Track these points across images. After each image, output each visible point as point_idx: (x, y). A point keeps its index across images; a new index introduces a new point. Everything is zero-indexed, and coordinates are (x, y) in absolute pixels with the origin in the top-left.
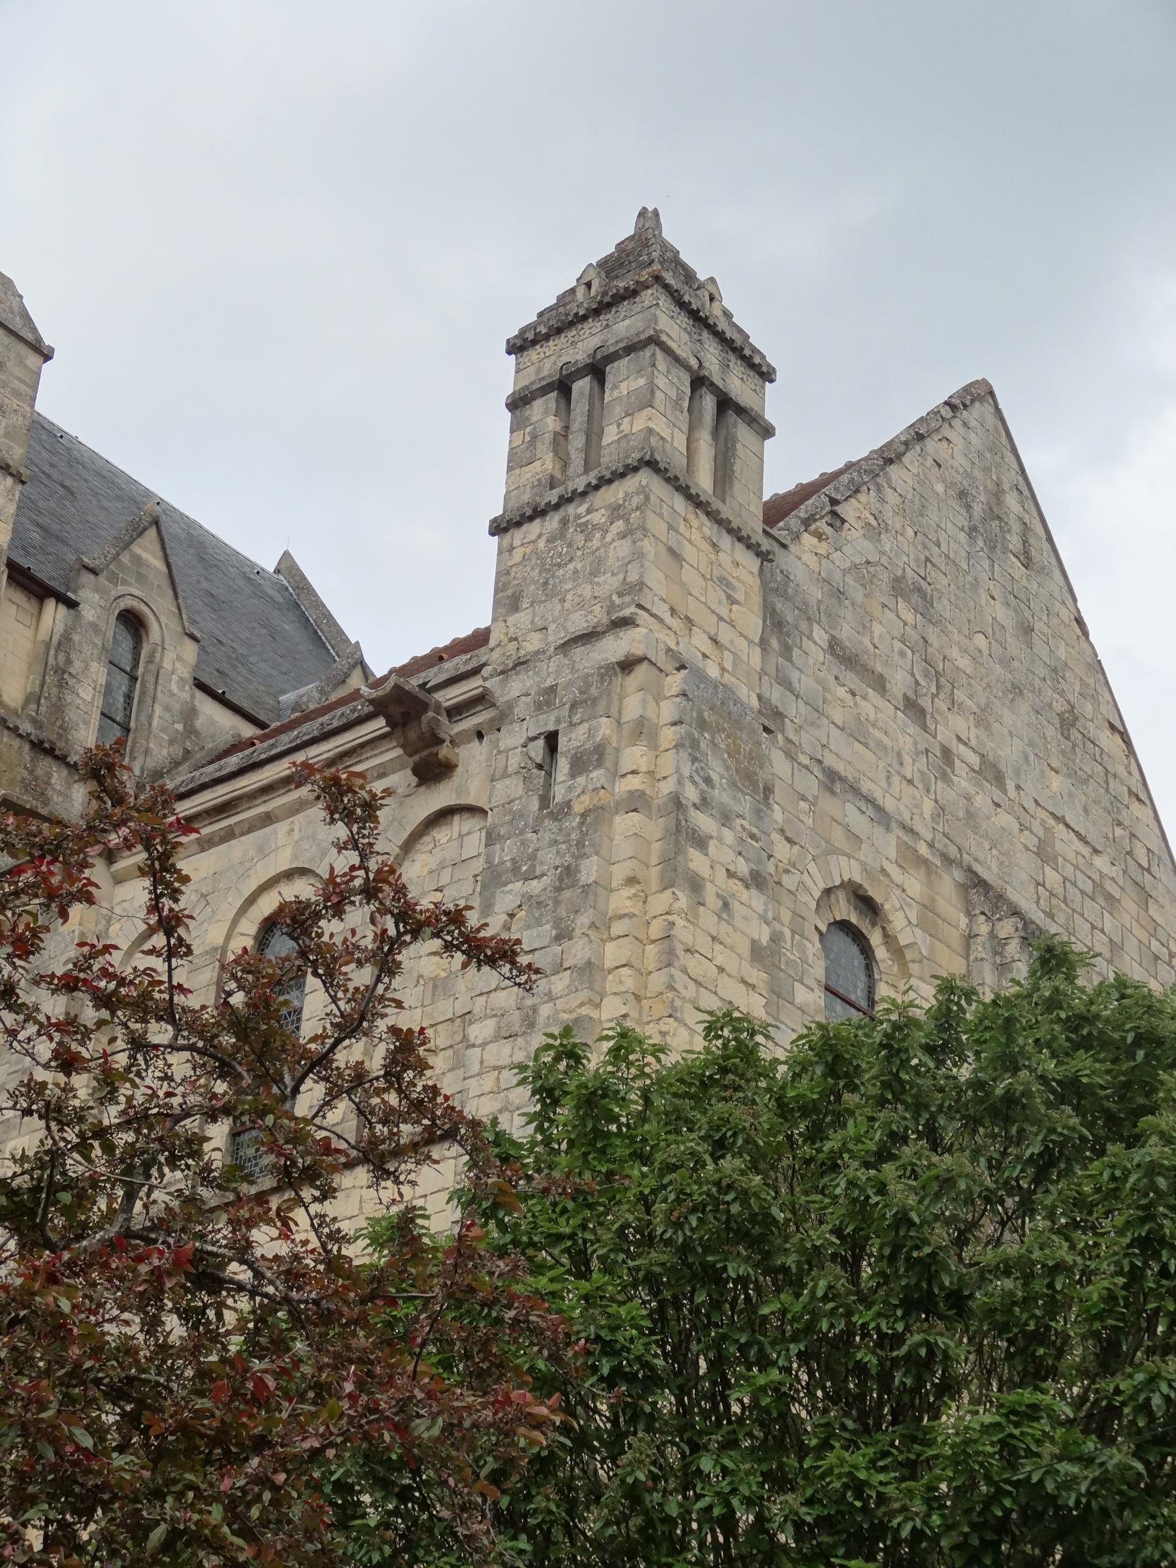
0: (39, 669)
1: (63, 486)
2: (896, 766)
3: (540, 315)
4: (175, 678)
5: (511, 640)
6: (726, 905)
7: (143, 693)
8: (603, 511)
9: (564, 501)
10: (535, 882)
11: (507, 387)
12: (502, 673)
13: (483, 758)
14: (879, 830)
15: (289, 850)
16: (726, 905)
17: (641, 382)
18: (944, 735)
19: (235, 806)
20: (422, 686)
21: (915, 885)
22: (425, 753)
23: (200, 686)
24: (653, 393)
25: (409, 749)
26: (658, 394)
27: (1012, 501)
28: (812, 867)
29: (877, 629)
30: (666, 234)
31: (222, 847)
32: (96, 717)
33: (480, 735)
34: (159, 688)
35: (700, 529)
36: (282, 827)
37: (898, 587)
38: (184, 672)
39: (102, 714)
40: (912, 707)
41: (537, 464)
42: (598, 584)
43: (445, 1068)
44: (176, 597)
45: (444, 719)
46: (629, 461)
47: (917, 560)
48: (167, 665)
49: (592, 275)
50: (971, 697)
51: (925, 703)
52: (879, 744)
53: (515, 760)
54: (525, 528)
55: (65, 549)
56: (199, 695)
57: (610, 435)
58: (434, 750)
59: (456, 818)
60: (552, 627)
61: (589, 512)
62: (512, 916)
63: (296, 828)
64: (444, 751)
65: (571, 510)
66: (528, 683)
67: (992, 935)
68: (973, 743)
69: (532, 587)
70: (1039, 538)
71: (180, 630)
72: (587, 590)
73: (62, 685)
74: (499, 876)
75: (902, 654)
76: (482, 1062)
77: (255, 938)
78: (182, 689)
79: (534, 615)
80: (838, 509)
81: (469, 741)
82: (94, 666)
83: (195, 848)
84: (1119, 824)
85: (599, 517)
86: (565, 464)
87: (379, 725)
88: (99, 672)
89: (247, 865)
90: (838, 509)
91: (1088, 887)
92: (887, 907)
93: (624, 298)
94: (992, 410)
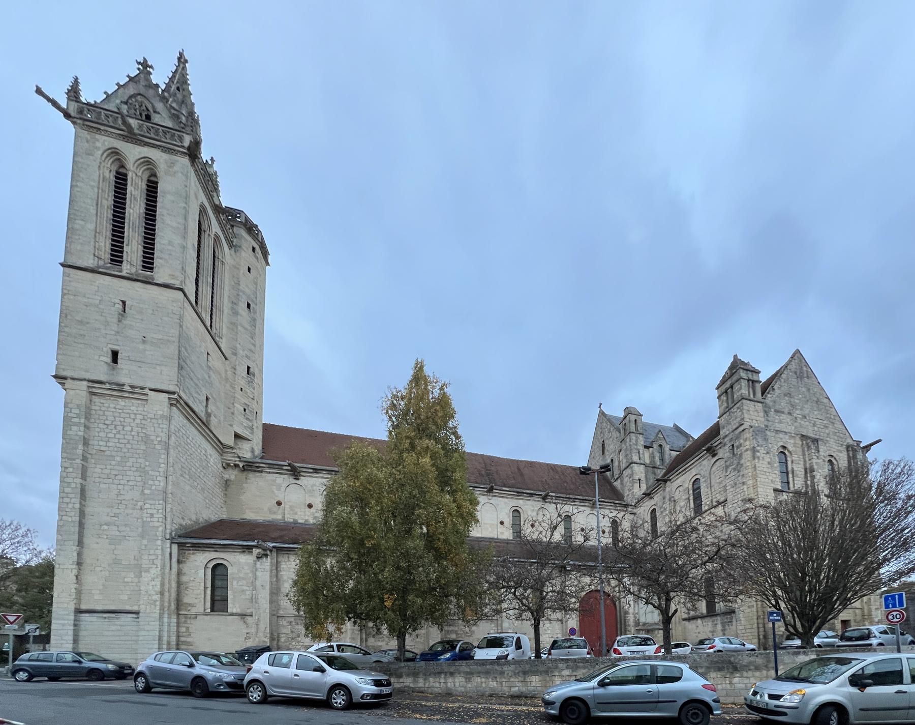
21: (792, 441)
23: (671, 450)
25: (710, 454)
27: (805, 368)
30: (739, 358)
37: (785, 395)
40: (790, 414)
51: (791, 412)
57: (735, 396)
64: (715, 452)
87: (705, 452)
88: (658, 454)
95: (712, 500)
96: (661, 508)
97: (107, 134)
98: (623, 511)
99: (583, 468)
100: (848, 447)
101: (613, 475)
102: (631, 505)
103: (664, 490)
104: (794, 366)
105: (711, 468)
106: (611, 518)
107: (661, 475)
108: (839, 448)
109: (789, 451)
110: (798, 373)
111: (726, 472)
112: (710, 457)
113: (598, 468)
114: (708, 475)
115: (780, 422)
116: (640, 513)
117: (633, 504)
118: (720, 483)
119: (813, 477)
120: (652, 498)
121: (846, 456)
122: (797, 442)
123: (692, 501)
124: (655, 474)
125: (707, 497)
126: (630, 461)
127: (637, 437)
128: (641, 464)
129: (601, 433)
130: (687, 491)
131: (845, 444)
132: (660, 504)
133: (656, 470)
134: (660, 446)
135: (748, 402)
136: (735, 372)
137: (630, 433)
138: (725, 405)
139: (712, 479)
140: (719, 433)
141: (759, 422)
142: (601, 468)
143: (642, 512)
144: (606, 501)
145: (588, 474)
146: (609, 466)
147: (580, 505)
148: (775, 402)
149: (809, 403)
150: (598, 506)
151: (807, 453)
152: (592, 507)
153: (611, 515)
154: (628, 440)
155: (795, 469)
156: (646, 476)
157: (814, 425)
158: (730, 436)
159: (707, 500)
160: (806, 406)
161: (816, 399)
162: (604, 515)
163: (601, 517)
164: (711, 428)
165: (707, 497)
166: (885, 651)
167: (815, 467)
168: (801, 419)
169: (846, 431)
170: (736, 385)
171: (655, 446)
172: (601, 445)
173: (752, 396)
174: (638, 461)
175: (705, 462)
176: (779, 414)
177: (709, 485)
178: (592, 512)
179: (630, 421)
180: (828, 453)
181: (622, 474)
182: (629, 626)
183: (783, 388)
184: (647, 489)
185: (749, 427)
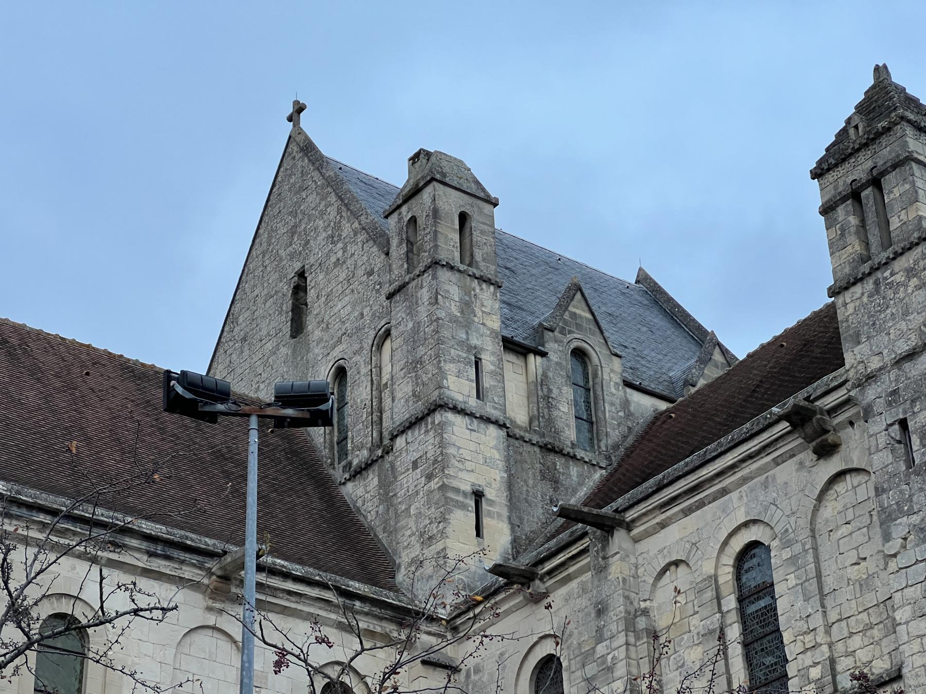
1: (507, 268)
3: (827, 150)
4: (612, 383)
5: (859, 363)
7: (596, 398)
8: (902, 273)
9: (873, 270)
10: (915, 516)
11: (817, 202)
12: (859, 386)
13: (857, 437)
15: (743, 509)
17: (907, 186)
19: (701, 487)
20: (807, 399)
22: (820, 440)
23: (628, 384)
24: (916, 192)
25: (808, 439)
26: (920, 191)
30: (895, 79)
31: (699, 512)
32: (573, 422)
33: (852, 424)
34: (605, 392)
36: (734, 495)
38: (617, 379)
39: (576, 417)
41: (849, 248)
42: (909, 320)
43: (881, 636)
44: (602, 333)
45: (826, 418)
46: (912, 239)
48: (606, 377)
49: (856, 120)
53: (882, 440)
54: (852, 289)
55: (524, 314)
56: (629, 390)
57: (895, 223)
58: (824, 437)
59: (848, 477)
60: (885, 352)
61: (892, 274)
62: (905, 539)
63: (744, 494)
64: (830, 438)
65: (879, 274)
66: (879, 390)
69: (866, 328)
71: (608, 353)
72: (903, 325)
73: (549, 407)
74: (890, 515)
76: (908, 634)
77: (734, 566)
78: (618, 389)
79: (871, 346)
81: (845, 428)
83: (681, 515)
85: (899, 278)
86: (867, 244)
87: (784, 426)
88: (568, 393)
89: (719, 521)
93: (882, 134)
95: (832, 662)
96: (587, 657)
97: (760, 613)
98: (389, 642)
99: (184, 377)
101: (343, 440)
102: (432, 619)
103: (601, 570)
105: (816, 509)
106: (318, 671)
107: (583, 493)
111: (887, 537)
112: (808, 456)
113: (267, 395)
114: (804, 534)
116: (477, 670)
117: (443, 613)
118: (864, 584)
120: (537, 599)
123: (736, 652)
124: (555, 482)
125: (809, 640)
126: (434, 396)
127: (467, 291)
128: (488, 420)
129: (293, 232)
130: (709, 594)
132: (580, 635)
133: (559, 462)
134: (580, 354)
136: (887, 130)
137: (436, 263)
138: (855, 247)
139: (823, 556)
140: (840, 362)
142: (285, 398)
143: (490, 666)
144: (298, 570)
145: (212, 417)
146: (324, 398)
147: (147, 573)
150: (252, 595)
153: (319, 656)
154: (424, 295)
156: (510, 485)
158: (886, 383)
159: (808, 659)
162: (283, 653)
163: (264, 658)
164: (803, 325)
165: (809, 640)
171: (557, 350)
172: (287, 290)
174: (472, 403)
175: (786, 472)
177: (813, 586)
178: (211, 620)
179: (435, 213)
181: (388, 451)
184: (517, 546)
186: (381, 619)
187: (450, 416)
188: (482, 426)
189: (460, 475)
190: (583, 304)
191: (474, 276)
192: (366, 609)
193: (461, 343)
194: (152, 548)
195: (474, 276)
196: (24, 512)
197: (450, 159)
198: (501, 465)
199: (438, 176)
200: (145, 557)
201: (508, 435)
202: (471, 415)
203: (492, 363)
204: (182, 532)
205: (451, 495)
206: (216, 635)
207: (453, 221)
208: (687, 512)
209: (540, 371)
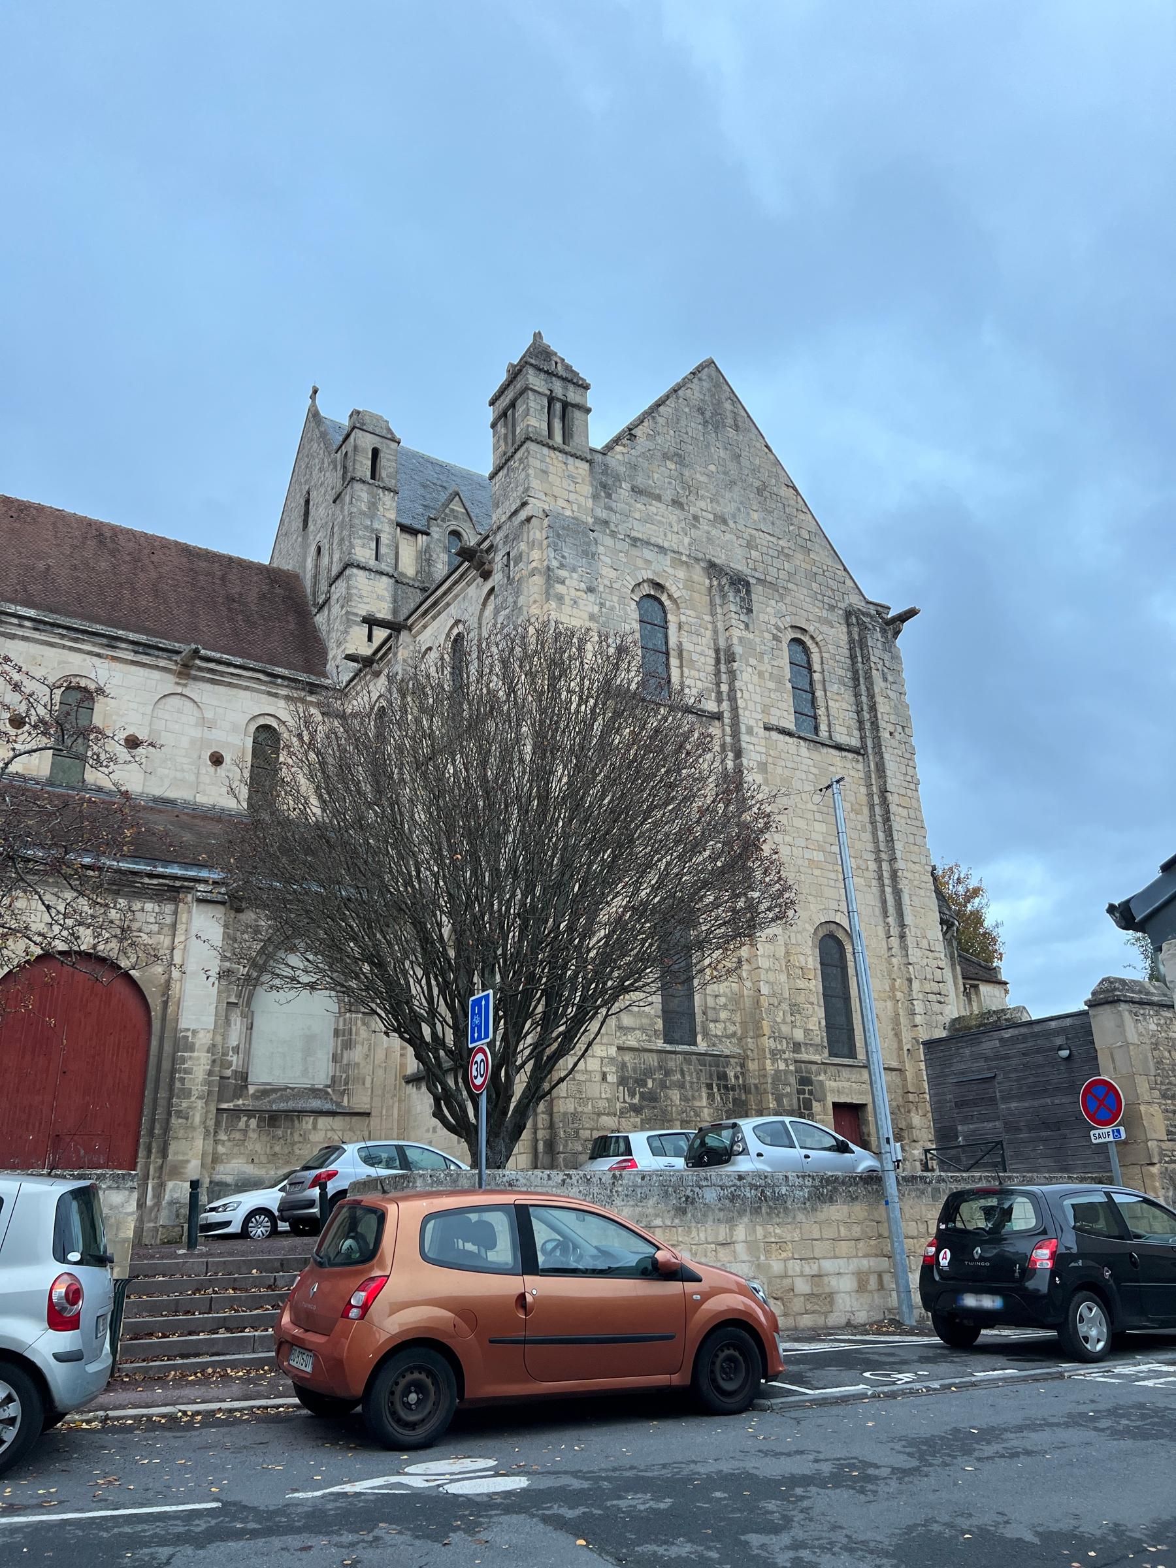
0: (419, 561)
2: (669, 528)
6: (575, 602)
14: (661, 557)
16: (575, 602)
18: (693, 510)
21: (681, 574)
27: (728, 406)
28: (628, 577)
29: (656, 476)
35: (557, 458)
37: (666, 457)
40: (676, 503)
47: (676, 443)
50: (708, 491)
51: (683, 500)
52: (660, 522)
57: (518, 431)
64: (486, 567)
65: (509, 464)
67: (719, 584)
68: (710, 510)
70: (743, 417)
75: (670, 483)
80: (633, 432)
82: (442, 555)
84: (792, 524)
90: (633, 432)
91: (775, 554)
92: (667, 584)
94: (714, 369)
100: (849, 614)
104: (697, 394)
108: (825, 613)
109: (670, 597)
110: (708, 414)
112: (480, 580)
115: (647, 520)
119: (732, 674)
121: (845, 637)
122: (696, 578)
128: (382, 573)
131: (842, 605)
135: (546, 450)
137: (353, 479)
141: (575, 507)
144: (238, 661)
148: (634, 467)
149: (736, 489)
151: (719, 610)
152: (180, 675)
155: (687, 646)
157: (750, 545)
160: (728, 495)
161: (757, 484)
166: (1073, 1183)
167: (738, 650)
168: (713, 523)
169: (844, 574)
170: (519, 402)
172: (302, 502)
173: (558, 438)
174: (372, 563)
175: (472, 591)
176: (644, 499)
178: (179, 690)
179: (356, 448)
180: (788, 620)
182: (187, 1093)
183: (659, 440)
185: (541, 515)
186: (297, 689)
187: (355, 571)
188: (378, 576)
189: (359, 605)
190: (460, 504)
191: (379, 487)
192: (286, 683)
193: (366, 528)
194: (136, 648)
195: (379, 487)
196: (48, 628)
197: (371, 415)
198: (389, 599)
199: (358, 425)
200: (132, 654)
201: (397, 581)
202: (370, 570)
203: (388, 539)
204: (158, 640)
205: (351, 617)
206: (183, 698)
207: (367, 454)
208: (434, 618)
209: (425, 544)
